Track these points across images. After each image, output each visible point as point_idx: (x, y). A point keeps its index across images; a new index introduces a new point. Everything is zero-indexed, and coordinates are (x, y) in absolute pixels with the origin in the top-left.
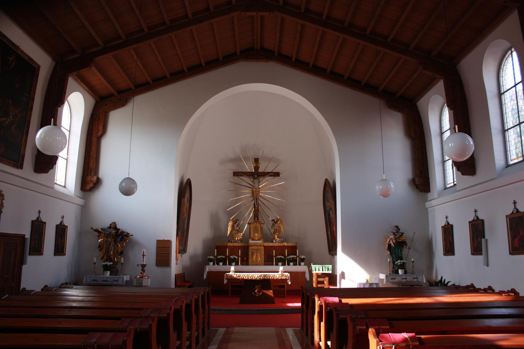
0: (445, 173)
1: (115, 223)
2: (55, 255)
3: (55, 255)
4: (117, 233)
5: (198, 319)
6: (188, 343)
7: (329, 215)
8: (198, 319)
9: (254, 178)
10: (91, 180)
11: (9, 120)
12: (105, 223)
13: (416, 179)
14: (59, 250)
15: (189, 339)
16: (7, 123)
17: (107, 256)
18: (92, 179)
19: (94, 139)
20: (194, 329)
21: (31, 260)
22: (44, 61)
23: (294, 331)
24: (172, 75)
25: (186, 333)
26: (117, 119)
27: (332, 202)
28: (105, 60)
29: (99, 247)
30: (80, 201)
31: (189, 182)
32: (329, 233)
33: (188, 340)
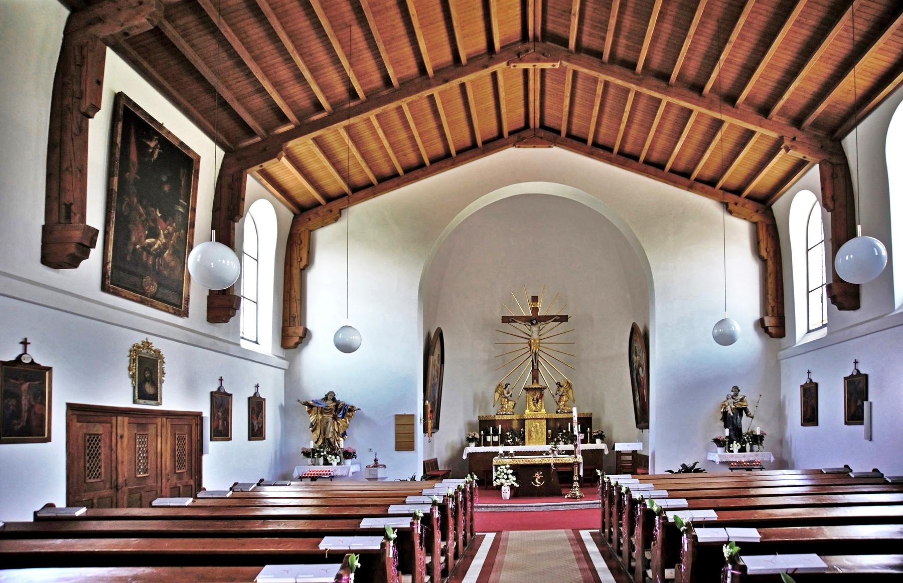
0: (810, 310)
1: (333, 392)
2: (249, 439)
3: (249, 439)
4: (337, 406)
5: (456, 524)
6: (443, 559)
7: (638, 373)
8: (456, 524)
9: (532, 324)
10: (294, 333)
11: (159, 242)
12: (316, 393)
13: (766, 319)
14: (256, 432)
15: (444, 552)
16: (156, 246)
17: (324, 439)
18: (297, 331)
19: (296, 272)
20: (451, 535)
21: (213, 450)
22: (209, 156)
23: (592, 534)
24: (407, 171)
25: (439, 544)
26: (326, 238)
27: (643, 356)
28: (303, 146)
29: (312, 425)
30: (284, 364)
31: (440, 334)
32: (637, 398)
33: (442, 555)
